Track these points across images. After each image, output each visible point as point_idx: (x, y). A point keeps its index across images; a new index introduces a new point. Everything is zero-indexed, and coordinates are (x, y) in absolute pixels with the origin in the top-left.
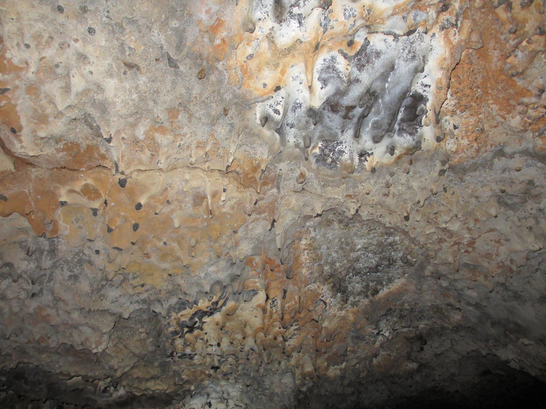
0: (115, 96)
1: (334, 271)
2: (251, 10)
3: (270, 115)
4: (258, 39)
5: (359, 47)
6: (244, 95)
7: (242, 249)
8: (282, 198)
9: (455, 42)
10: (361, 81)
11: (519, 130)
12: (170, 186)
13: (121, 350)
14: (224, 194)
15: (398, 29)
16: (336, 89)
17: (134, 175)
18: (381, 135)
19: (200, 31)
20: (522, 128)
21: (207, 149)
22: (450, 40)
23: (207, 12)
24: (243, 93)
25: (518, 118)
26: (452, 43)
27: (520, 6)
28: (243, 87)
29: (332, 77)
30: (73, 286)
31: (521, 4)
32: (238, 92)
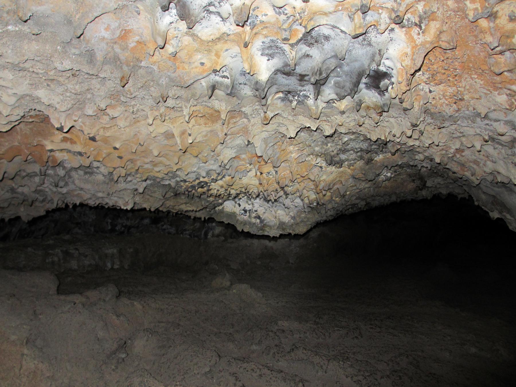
0: (50, 99)
1: (325, 151)
2: (156, 21)
3: (217, 82)
4: (177, 37)
5: (301, 36)
6: (180, 78)
7: (226, 154)
8: (252, 126)
9: (419, 42)
10: (311, 57)
11: (504, 107)
12: (138, 132)
13: (148, 199)
14: (190, 138)
15: (344, 26)
16: (284, 63)
17: (101, 132)
18: (343, 94)
19: (107, 44)
20: (508, 107)
21: (161, 112)
22: (413, 38)
23: (106, 29)
24: (179, 76)
25: (504, 97)
26: (415, 42)
27: (507, 18)
28: (177, 70)
29: (277, 53)
30: (90, 178)
31: (509, 16)
32: (173, 75)
